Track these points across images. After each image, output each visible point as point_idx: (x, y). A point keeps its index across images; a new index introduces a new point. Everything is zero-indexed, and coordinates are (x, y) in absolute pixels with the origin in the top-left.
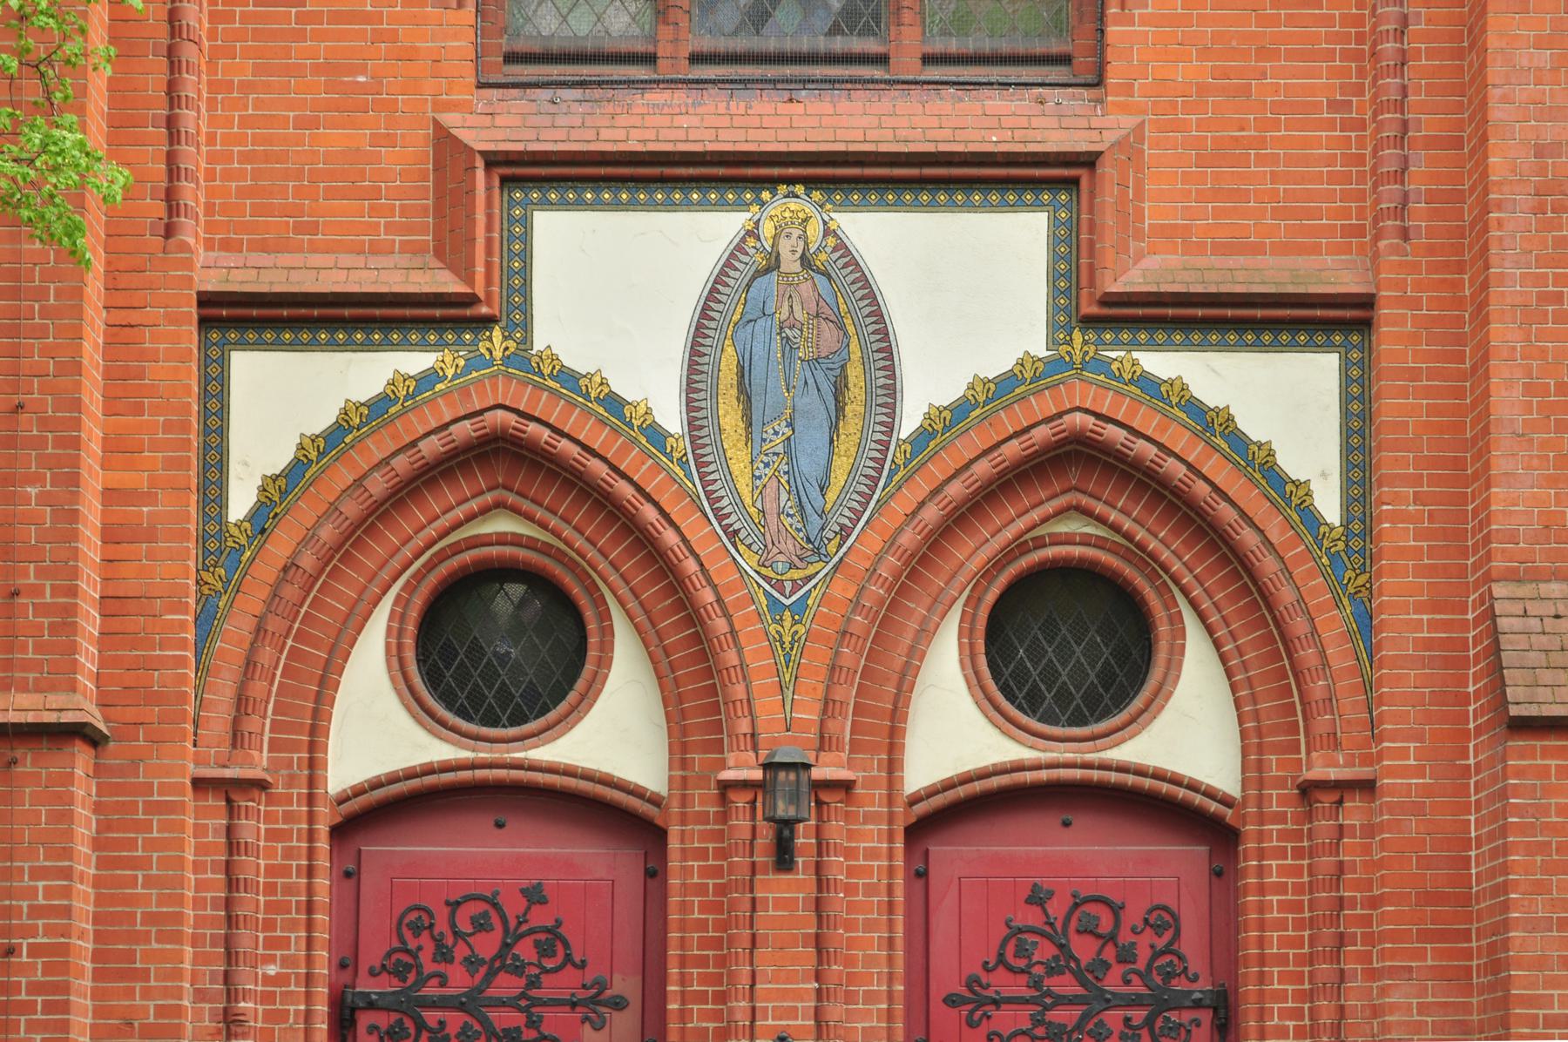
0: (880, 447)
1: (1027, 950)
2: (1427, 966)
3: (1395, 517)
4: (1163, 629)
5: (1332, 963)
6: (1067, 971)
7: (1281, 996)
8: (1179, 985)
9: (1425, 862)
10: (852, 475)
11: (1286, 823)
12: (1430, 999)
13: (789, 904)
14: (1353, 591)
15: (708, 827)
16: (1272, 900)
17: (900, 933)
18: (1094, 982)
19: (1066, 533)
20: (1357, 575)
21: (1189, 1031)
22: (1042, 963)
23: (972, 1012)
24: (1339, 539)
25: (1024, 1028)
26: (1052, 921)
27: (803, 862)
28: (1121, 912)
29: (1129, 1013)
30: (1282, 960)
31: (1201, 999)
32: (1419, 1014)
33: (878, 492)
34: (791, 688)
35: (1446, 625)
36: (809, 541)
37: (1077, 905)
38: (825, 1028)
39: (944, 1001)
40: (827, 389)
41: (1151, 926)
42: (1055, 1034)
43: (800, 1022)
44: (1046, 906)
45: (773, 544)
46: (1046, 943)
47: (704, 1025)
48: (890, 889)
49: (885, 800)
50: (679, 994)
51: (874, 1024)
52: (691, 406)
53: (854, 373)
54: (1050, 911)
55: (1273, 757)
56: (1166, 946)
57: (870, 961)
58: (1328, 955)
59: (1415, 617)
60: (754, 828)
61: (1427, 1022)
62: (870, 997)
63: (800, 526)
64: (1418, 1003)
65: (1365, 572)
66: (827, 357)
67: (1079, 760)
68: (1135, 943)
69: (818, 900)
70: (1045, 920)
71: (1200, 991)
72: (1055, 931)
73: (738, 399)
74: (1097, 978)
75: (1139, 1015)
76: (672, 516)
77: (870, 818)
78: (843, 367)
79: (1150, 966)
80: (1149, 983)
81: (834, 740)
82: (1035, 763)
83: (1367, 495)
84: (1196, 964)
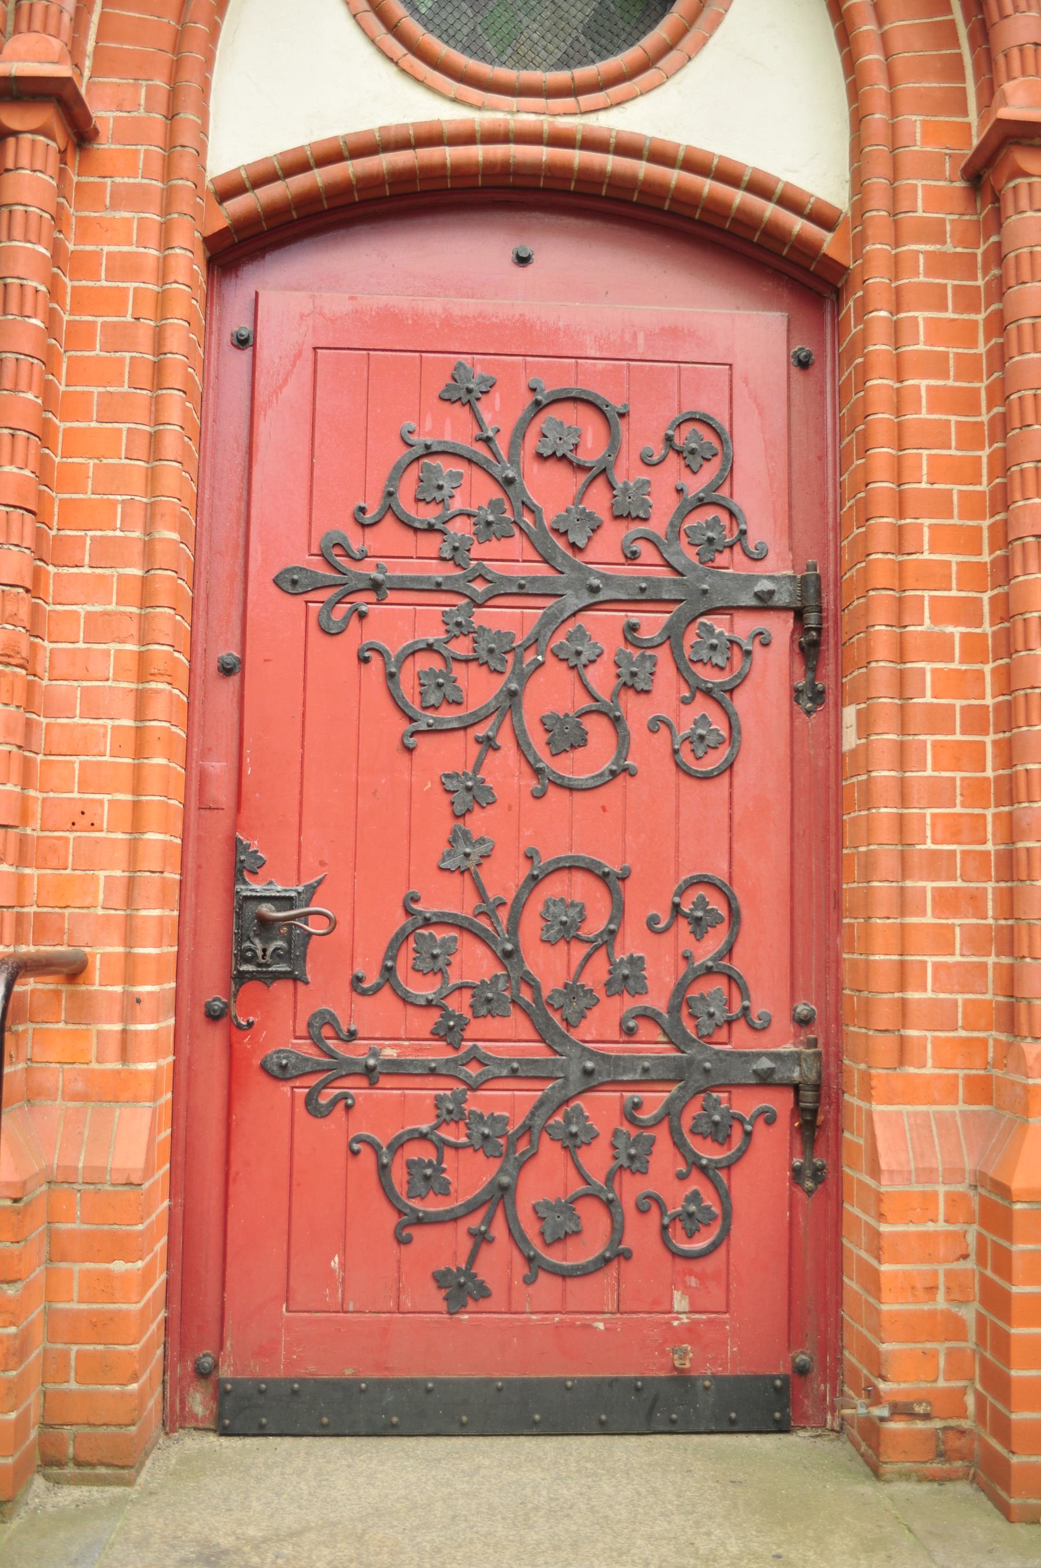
1: (440, 488)
6: (516, 531)
7: (938, 576)
11: (944, 243)
16: (918, 387)
18: (569, 553)
21: (748, 653)
22: (469, 515)
25: (431, 640)
26: (490, 434)
28: (622, 425)
29: (634, 617)
30: (941, 504)
31: (771, 593)
37: (539, 407)
41: (679, 453)
42: (491, 651)
44: (479, 406)
46: (478, 475)
48: (159, 337)
49: (157, 166)
51: (112, 607)
54: (487, 417)
67: (546, 127)
68: (648, 482)
70: (477, 432)
71: (771, 578)
74: (573, 546)
77: (123, 198)
79: (675, 529)
80: (672, 560)
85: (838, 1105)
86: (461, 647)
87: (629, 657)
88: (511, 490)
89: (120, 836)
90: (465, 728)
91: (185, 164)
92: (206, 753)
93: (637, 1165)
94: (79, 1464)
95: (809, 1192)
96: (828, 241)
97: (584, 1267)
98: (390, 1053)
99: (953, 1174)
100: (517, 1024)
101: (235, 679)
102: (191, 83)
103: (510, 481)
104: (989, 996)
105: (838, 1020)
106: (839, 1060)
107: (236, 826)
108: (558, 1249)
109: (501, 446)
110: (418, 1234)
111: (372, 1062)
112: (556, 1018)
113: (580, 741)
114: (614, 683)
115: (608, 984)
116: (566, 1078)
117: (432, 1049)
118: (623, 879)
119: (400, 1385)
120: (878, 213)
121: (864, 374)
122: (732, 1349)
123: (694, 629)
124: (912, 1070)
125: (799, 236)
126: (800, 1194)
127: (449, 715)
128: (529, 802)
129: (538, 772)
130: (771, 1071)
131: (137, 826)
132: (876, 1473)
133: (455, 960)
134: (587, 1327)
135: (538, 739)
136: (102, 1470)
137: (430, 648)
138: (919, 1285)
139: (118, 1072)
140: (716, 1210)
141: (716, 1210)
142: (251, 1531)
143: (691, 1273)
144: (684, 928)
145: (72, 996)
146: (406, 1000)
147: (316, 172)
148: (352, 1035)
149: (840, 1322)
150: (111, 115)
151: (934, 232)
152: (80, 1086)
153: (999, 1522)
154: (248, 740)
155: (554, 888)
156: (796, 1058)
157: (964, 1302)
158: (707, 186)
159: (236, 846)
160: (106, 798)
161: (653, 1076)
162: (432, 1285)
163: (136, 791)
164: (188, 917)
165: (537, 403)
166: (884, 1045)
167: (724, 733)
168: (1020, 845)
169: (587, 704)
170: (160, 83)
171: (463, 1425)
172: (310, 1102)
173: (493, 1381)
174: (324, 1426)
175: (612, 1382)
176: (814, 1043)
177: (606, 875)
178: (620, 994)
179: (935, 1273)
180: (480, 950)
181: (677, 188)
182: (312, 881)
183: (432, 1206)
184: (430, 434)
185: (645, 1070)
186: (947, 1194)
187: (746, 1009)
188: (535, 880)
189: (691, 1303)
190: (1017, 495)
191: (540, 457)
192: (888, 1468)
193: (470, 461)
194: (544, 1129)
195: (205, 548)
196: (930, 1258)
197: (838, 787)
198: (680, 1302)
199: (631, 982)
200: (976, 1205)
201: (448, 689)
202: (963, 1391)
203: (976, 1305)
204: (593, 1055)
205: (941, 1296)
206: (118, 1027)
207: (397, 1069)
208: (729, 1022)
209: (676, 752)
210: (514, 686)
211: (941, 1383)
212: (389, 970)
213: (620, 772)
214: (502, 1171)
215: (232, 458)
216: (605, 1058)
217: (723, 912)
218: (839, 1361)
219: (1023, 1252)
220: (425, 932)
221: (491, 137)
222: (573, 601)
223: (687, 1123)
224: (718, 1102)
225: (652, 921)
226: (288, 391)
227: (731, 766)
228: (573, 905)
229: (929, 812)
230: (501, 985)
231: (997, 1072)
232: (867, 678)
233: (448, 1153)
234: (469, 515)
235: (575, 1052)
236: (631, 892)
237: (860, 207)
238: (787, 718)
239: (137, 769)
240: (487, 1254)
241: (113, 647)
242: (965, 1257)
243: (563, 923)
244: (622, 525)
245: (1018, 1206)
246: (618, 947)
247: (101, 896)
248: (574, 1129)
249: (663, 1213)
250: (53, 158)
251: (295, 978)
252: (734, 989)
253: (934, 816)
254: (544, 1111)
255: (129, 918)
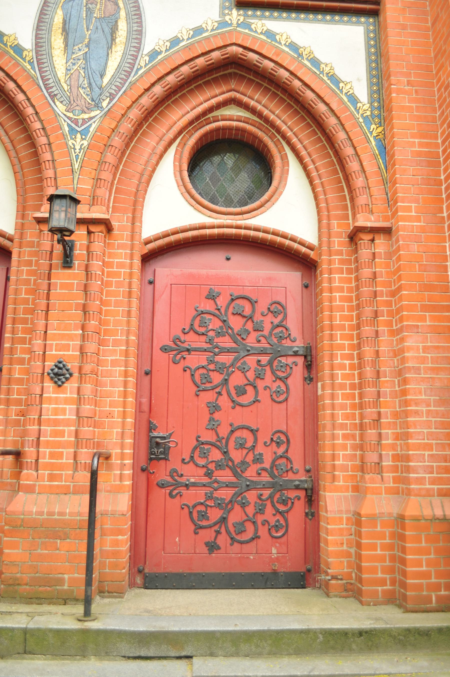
0: (133, 58)
1: (206, 323)
2: (427, 325)
3: (399, 91)
4: (278, 161)
5: (371, 326)
6: (227, 334)
7: (342, 347)
8: (287, 343)
9: (423, 268)
10: (118, 70)
11: (343, 256)
12: (429, 344)
13: (69, 286)
14: (375, 135)
15: (34, 249)
17: (134, 309)
18: (241, 340)
19: (229, 115)
20: (377, 127)
21: (291, 368)
22: (214, 330)
23: (176, 356)
24: (367, 110)
25: (203, 365)
27: (78, 263)
28: (256, 305)
29: (260, 358)
30: (343, 327)
31: (297, 351)
32: (424, 352)
33: (130, 78)
34: (78, 172)
35: (427, 145)
36: (93, 100)
37: (233, 300)
38: (85, 357)
39: (161, 349)
40: (107, 30)
41: (272, 312)
42: (220, 368)
43: (70, 353)
44: (216, 300)
45: (74, 101)
46: (216, 319)
47: (23, 356)
48: (130, 284)
49: (129, 238)
50: (11, 339)
51: (118, 358)
52: (37, 37)
53: (122, 25)
54: (218, 303)
55: (335, 222)
56: (279, 323)
57: (117, 323)
58: (369, 322)
59: (411, 140)
60: (53, 245)
61: (428, 357)
62: (116, 343)
63: (89, 93)
64: (423, 346)
65: (381, 126)
66: (109, 17)
69: (86, 286)
70: (216, 307)
71: (298, 347)
72: (221, 313)
73: (62, 34)
74: (243, 338)
75: (265, 359)
76: (23, 87)
77: (120, 246)
78: (116, 22)
79: (271, 334)
80: (270, 342)
81: (99, 199)
82: (212, 224)
83: (381, 90)
84: (295, 332)
85: (318, 494)
86: (212, 367)
87: (258, 369)
88: (225, 323)
89: (120, 420)
90: (213, 389)
91: (137, 237)
92: (141, 396)
93: (261, 512)
94: (109, 592)
95: (310, 520)
96: (312, 254)
97: (247, 541)
98: (192, 480)
99: (348, 512)
100: (228, 472)
101: (149, 376)
102: (138, 215)
103: (225, 321)
104: (357, 463)
105: (318, 471)
106: (318, 482)
107: (150, 417)
108: (240, 535)
109: (223, 311)
110: (200, 531)
111: (187, 483)
112: (239, 470)
113: (244, 393)
114: (254, 377)
115: (253, 461)
116: (241, 487)
117: (204, 479)
118: (257, 431)
119: (195, 574)
120: (325, 248)
121: (322, 291)
122: (289, 564)
123: (276, 361)
124: (336, 483)
125: (304, 253)
126: (308, 520)
127: (208, 386)
128: (231, 410)
129: (233, 401)
130: (299, 485)
131: (124, 417)
132: (328, 595)
133: (210, 454)
134: (248, 558)
135: (233, 392)
136: (115, 594)
137: (203, 367)
138: (339, 543)
139: (119, 485)
140: (284, 524)
141: (284, 524)
142: (157, 607)
143: (277, 542)
144: (274, 444)
145: (107, 464)
146: (197, 465)
147: (171, 236)
148: (182, 475)
149: (319, 556)
150: (117, 224)
151: (340, 253)
152: (109, 488)
153: (359, 606)
154: (153, 393)
155: (238, 434)
156: (306, 481)
157: (351, 547)
158: (279, 239)
159: (150, 422)
160: (116, 409)
161: (266, 486)
162: (204, 546)
163: (124, 407)
164: (136, 442)
165: (232, 299)
166: (329, 476)
167: (285, 390)
168: (364, 421)
169: (247, 382)
170: (130, 215)
171: (213, 586)
172: (170, 494)
173: (222, 573)
174: (174, 586)
175: (255, 574)
176: (311, 477)
177: (252, 430)
178: (257, 463)
179: (343, 539)
180: (217, 451)
181: (270, 240)
182: (171, 432)
183: (204, 523)
184: (203, 308)
185: (264, 485)
186: (346, 517)
187: (292, 468)
188: (232, 431)
189: (277, 551)
190: (362, 326)
191: (233, 314)
192: (331, 594)
193: (214, 315)
194: (235, 501)
195: (141, 340)
196: (342, 535)
197: (317, 405)
198: (274, 551)
199: (259, 460)
200: (354, 520)
201: (208, 379)
202: (352, 572)
203: (355, 548)
204: (249, 480)
205: (345, 545)
206: (119, 472)
207: (194, 485)
208: (287, 471)
209: (271, 395)
210: (226, 378)
211: (345, 570)
212: (192, 457)
213: (256, 401)
214: (224, 513)
215: (148, 315)
216: (252, 481)
217: (285, 440)
218: (319, 567)
219: (365, 531)
220: (202, 446)
221: (219, 227)
222: (243, 354)
223: (275, 500)
224: (284, 494)
225: (265, 443)
226: (164, 296)
227: (287, 399)
228: (243, 438)
229: (340, 412)
230: (223, 461)
231: (360, 484)
232: (323, 375)
233: (209, 509)
234: (214, 330)
235: (244, 480)
236: (259, 435)
237: (320, 245)
238: (302, 386)
239: (124, 402)
240: (220, 537)
241: (118, 368)
242: (351, 535)
243: (240, 444)
244: (256, 332)
245: (363, 519)
246: (256, 450)
247: (115, 436)
248: (244, 501)
249: (269, 525)
250: (103, 237)
251: (166, 459)
252: (289, 463)
253: (342, 413)
254: (235, 496)
255: (122, 442)
